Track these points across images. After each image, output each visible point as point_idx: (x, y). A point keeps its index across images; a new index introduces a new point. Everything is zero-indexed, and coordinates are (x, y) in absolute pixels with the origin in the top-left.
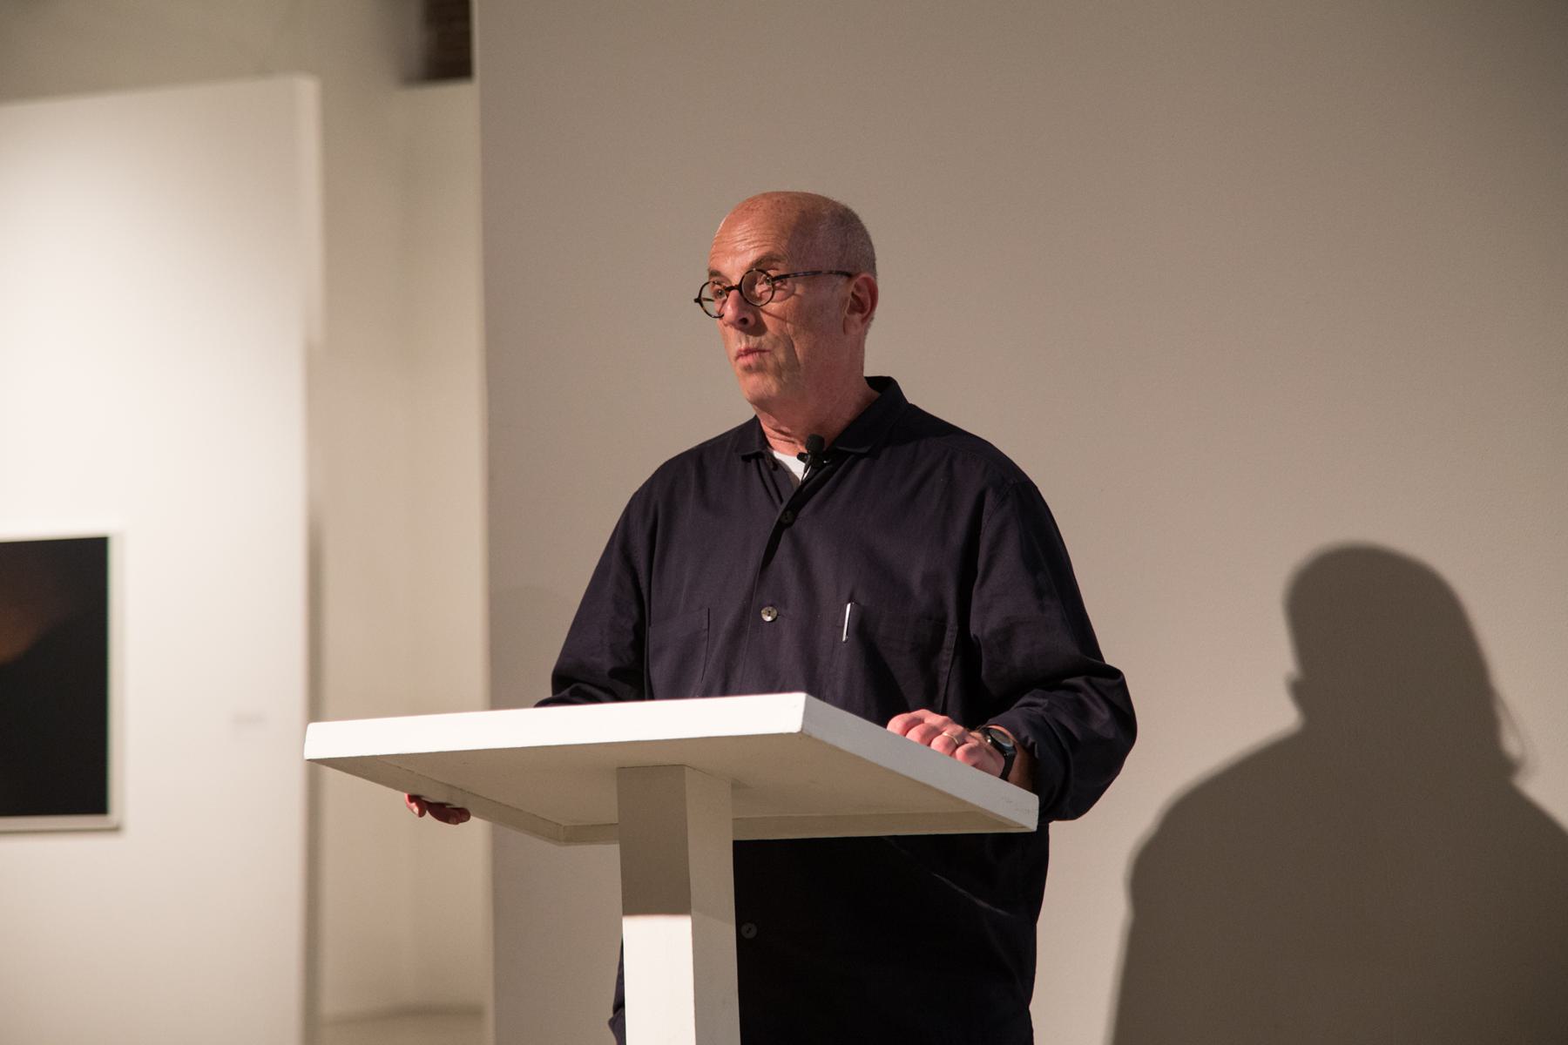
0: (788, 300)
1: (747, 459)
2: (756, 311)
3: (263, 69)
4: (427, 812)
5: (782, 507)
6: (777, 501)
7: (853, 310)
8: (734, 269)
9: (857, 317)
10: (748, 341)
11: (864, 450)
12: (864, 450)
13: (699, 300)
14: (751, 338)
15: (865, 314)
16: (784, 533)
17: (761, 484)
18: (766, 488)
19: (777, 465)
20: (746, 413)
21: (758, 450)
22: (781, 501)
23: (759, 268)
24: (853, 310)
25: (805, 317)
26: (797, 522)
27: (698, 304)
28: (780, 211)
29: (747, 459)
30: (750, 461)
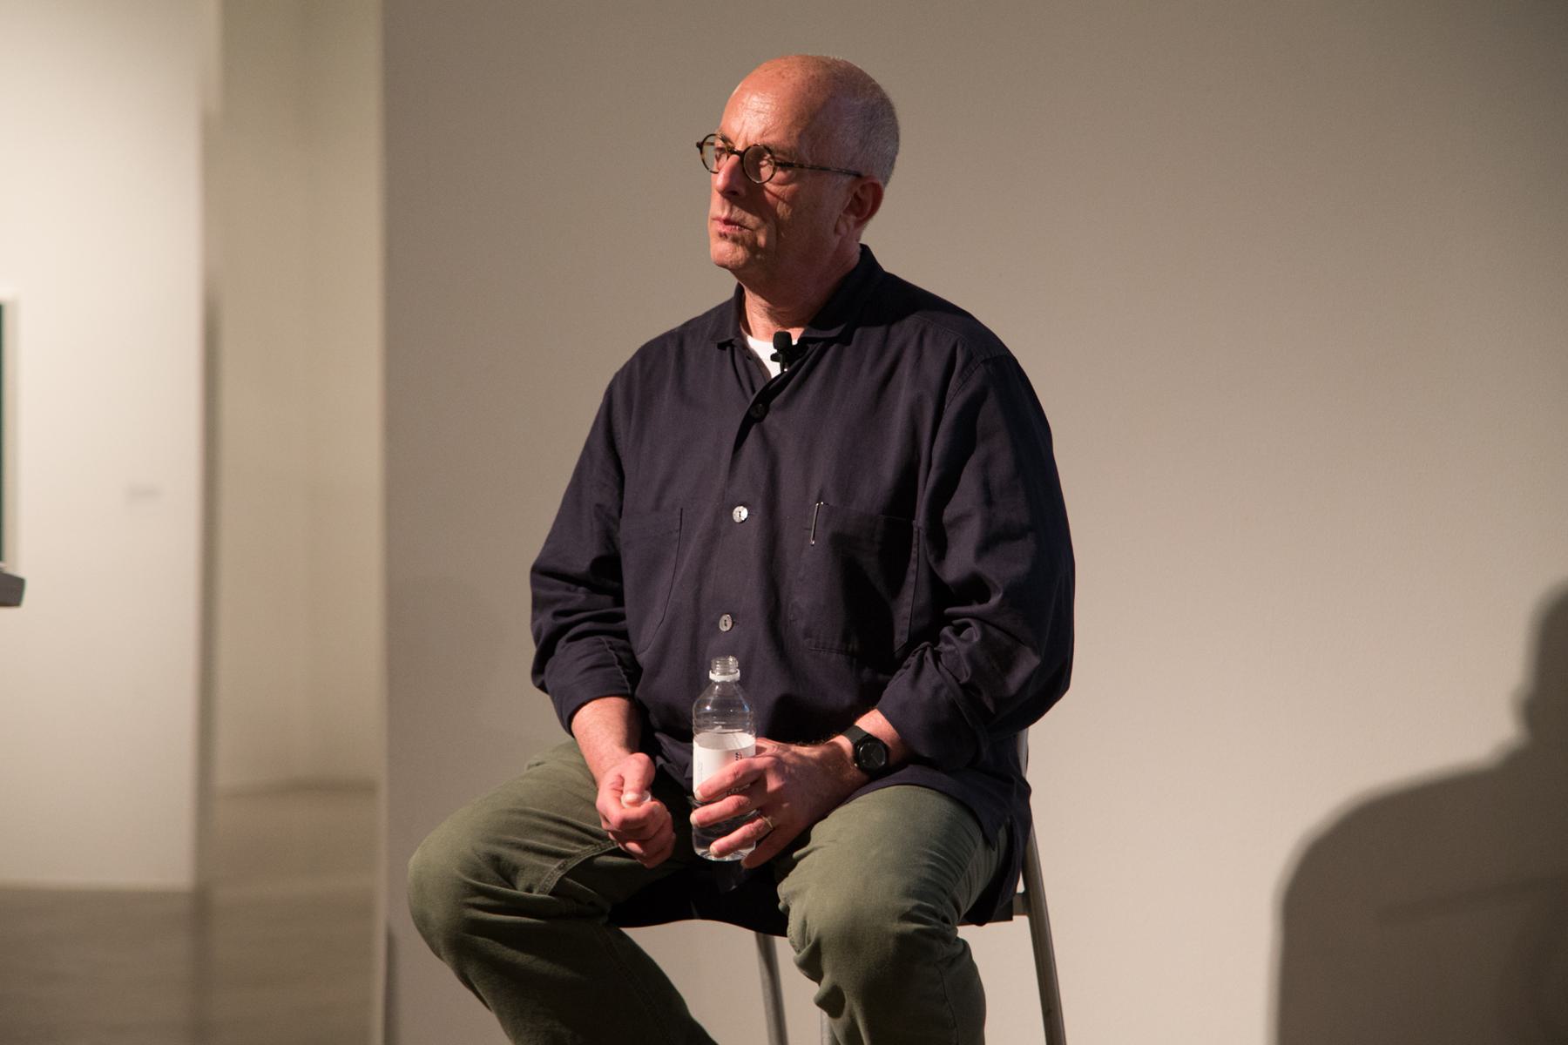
0: (784, 187)
1: (722, 346)
5: (752, 398)
6: (748, 390)
7: (850, 209)
9: (852, 218)
10: (731, 210)
11: (834, 333)
12: (834, 333)
13: (700, 146)
14: (736, 209)
15: (861, 218)
16: (754, 427)
17: (735, 379)
18: (738, 376)
21: (731, 337)
22: (754, 391)
26: (768, 416)
27: (698, 150)
28: (809, 92)
29: (722, 346)
30: (725, 349)
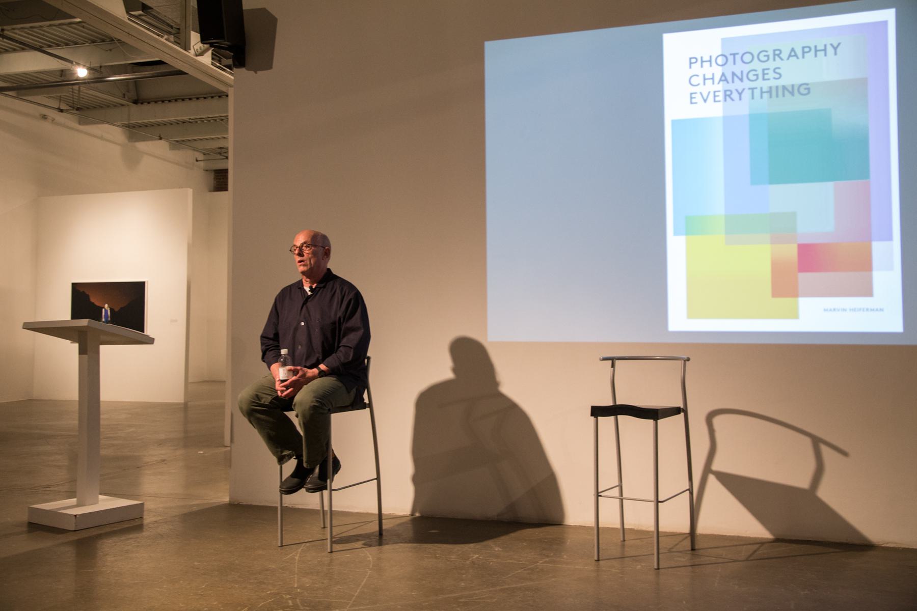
2: (302, 252)
3: (181, 187)
4: (286, 413)
5: (304, 299)
7: (325, 255)
8: (298, 244)
9: (326, 256)
13: (290, 251)
19: (305, 291)
20: (299, 277)
23: (302, 245)
24: (325, 255)
25: (314, 254)
